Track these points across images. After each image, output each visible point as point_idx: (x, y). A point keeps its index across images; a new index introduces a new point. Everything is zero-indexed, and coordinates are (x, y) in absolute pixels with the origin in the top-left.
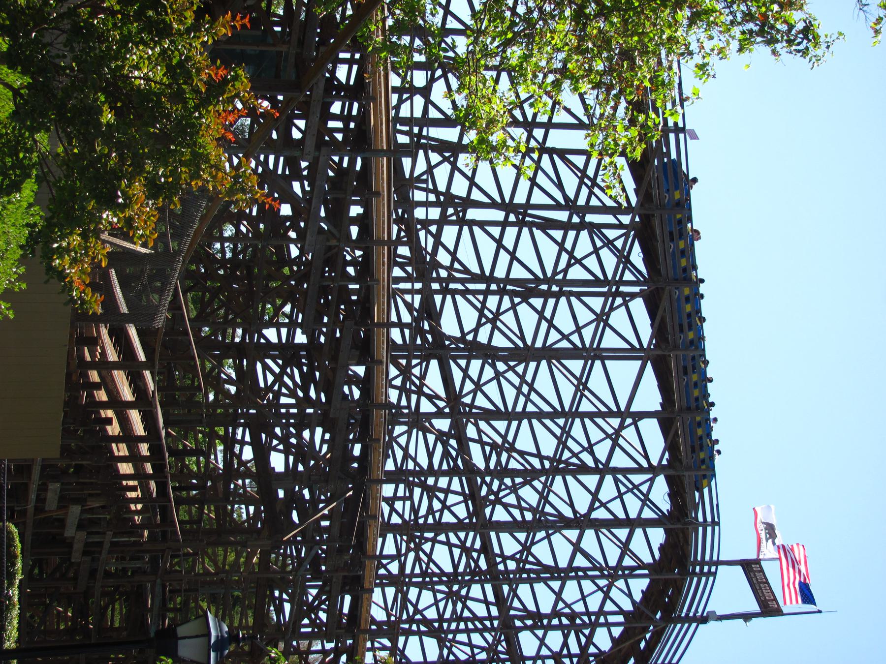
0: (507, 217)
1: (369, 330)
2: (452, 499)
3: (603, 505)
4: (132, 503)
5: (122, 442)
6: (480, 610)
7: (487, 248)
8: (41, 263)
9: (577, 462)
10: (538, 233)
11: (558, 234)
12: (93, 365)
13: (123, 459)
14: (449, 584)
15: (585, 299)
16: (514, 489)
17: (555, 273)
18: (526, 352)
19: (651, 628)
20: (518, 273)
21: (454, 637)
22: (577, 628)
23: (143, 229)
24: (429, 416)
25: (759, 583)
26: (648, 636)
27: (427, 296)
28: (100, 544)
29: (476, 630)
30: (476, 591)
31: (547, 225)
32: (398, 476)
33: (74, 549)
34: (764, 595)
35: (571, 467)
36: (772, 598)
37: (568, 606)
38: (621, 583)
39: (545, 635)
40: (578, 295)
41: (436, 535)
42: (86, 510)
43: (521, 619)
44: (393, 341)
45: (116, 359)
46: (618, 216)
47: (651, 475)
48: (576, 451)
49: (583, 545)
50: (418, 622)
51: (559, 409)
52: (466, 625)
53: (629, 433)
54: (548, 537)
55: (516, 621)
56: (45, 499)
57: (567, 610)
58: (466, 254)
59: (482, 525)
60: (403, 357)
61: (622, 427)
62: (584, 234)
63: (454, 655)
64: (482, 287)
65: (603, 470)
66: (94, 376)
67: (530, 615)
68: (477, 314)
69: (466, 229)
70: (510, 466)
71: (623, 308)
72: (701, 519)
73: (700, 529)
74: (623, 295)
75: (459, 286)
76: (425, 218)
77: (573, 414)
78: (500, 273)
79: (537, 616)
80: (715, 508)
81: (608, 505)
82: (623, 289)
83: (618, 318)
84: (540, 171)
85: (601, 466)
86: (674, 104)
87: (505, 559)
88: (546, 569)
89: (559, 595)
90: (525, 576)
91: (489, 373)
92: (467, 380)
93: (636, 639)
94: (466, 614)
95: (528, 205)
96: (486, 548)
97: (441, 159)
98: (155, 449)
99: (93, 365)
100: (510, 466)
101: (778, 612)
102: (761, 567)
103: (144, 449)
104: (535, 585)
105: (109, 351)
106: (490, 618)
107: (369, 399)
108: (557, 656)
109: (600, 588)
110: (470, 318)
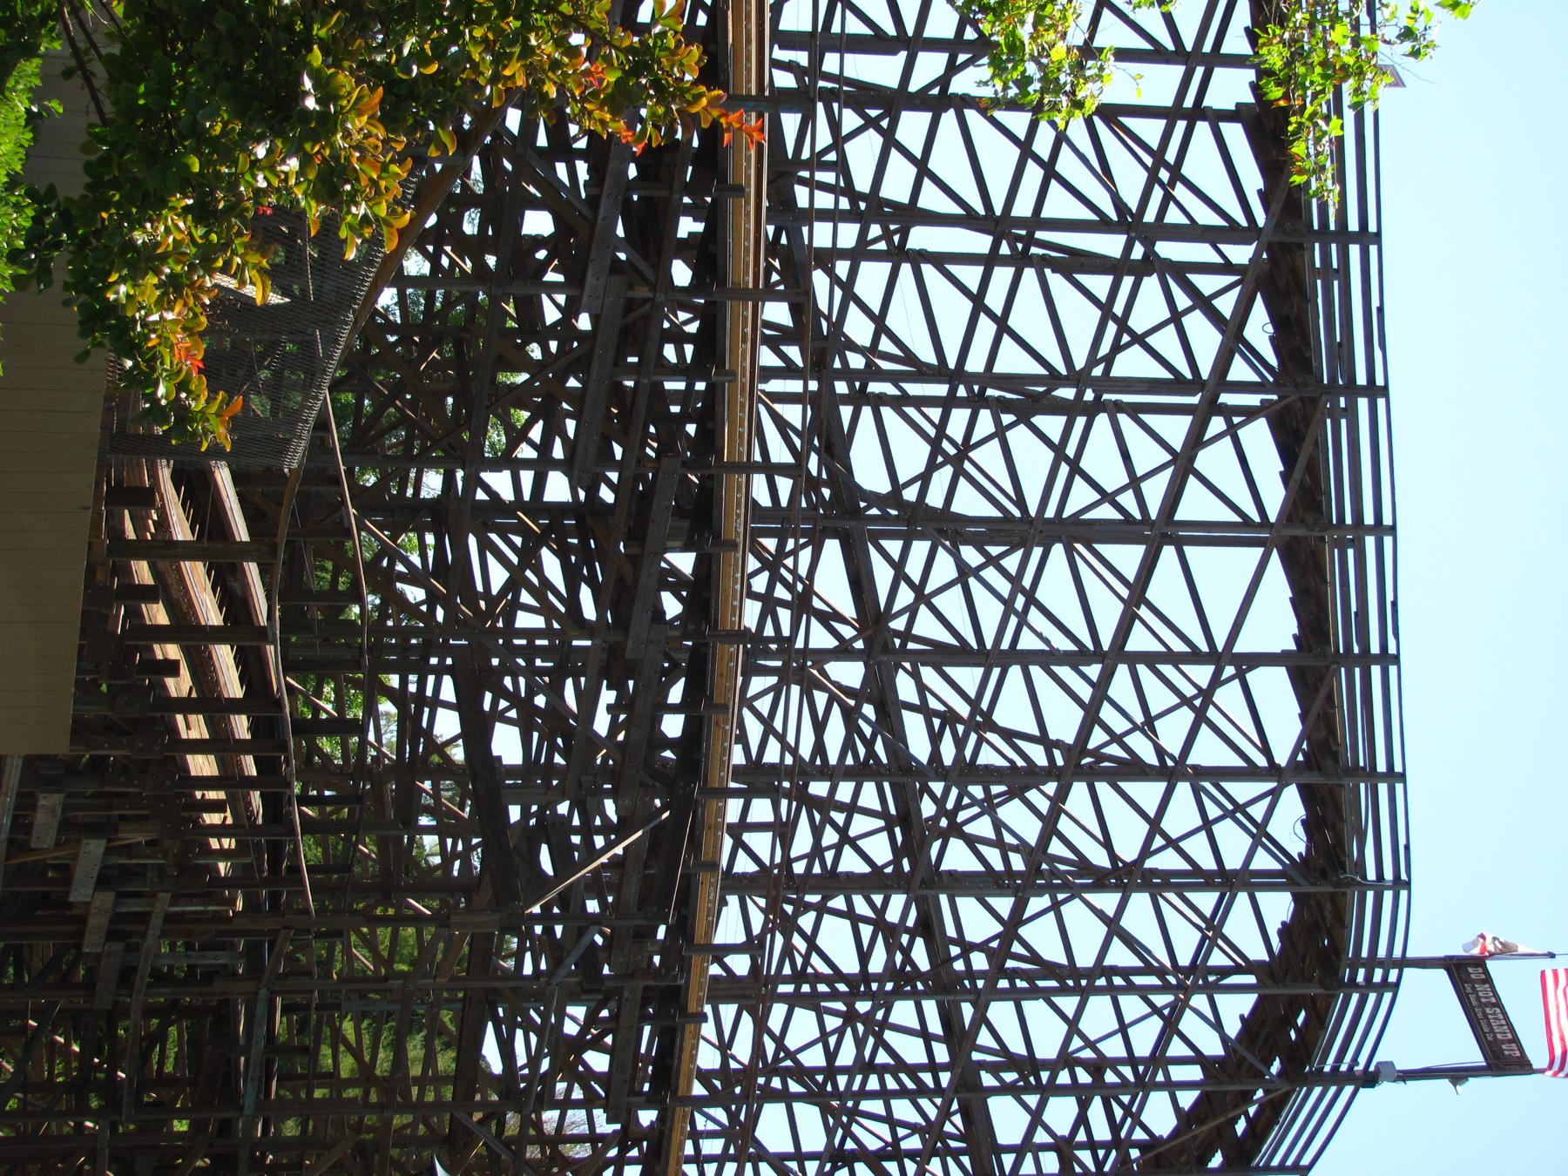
0: (995, 246)
1: (711, 477)
2: (860, 824)
3: (1172, 843)
4: (213, 837)
5: (196, 712)
6: (912, 1050)
7: (952, 310)
8: (67, 303)
9: (1122, 754)
10: (1056, 281)
11: (1100, 284)
12: (140, 549)
13: (198, 747)
14: (850, 999)
15: (1149, 419)
16: (989, 807)
17: (1092, 361)
18: (1026, 527)
19: (1260, 1093)
20: (1012, 361)
21: (857, 1104)
22: (1105, 1092)
23: (368, 200)
24: (824, 656)
25: (1482, 1005)
26: (1252, 1110)
27: (822, 407)
28: (144, 918)
29: (903, 1092)
30: (903, 1012)
31: (1075, 264)
32: (758, 779)
33: (90, 926)
34: (1492, 1031)
35: (1106, 764)
36: (1510, 1036)
37: (1090, 1044)
38: (1199, 1001)
39: (1042, 1105)
40: (1134, 411)
41: (826, 899)
42: (116, 847)
43: (995, 1069)
44: (755, 502)
45: (190, 537)
46: (1221, 246)
47: (1274, 785)
48: (1118, 731)
49: (1126, 922)
50: (785, 1074)
51: (1090, 646)
52: (882, 1082)
53: (1229, 697)
54: (1056, 907)
55: (983, 1074)
56: (31, 825)
57: (1088, 1054)
58: (906, 320)
59: (923, 882)
60: (769, 533)
61: (1216, 682)
62: (1151, 284)
63: (856, 1140)
64: (941, 390)
65: (1171, 771)
66: (142, 572)
67: (1011, 1061)
68: (927, 448)
69: (906, 269)
70: (981, 761)
71: (1227, 440)
72: (1371, 875)
73: (1370, 895)
74: (1228, 412)
75: (888, 389)
76: (829, 245)
77: (1116, 655)
78: (976, 364)
79: (1028, 1064)
80: (1403, 854)
81: (1182, 844)
82: (1226, 398)
83: (1216, 460)
84: (1064, 145)
85: (1170, 763)
86: (339, 283)
87: (968, 948)
88: (1050, 969)
89: (1073, 1024)
90: (1003, 984)
91: (945, 568)
92: (917, 581)
93: (1230, 1116)
94: (882, 1057)
95: (1037, 221)
96: (928, 927)
97: (860, 122)
98: (265, 729)
99: (140, 549)
100: (981, 761)
101: (1521, 1066)
102: (1486, 972)
103: (241, 726)
104: (1026, 1004)
105: (175, 518)
106: (933, 1067)
107: (708, 621)
108: (1064, 1147)
109: (1156, 1010)
110: (912, 455)
